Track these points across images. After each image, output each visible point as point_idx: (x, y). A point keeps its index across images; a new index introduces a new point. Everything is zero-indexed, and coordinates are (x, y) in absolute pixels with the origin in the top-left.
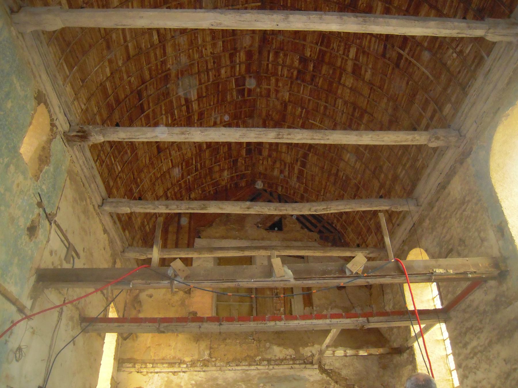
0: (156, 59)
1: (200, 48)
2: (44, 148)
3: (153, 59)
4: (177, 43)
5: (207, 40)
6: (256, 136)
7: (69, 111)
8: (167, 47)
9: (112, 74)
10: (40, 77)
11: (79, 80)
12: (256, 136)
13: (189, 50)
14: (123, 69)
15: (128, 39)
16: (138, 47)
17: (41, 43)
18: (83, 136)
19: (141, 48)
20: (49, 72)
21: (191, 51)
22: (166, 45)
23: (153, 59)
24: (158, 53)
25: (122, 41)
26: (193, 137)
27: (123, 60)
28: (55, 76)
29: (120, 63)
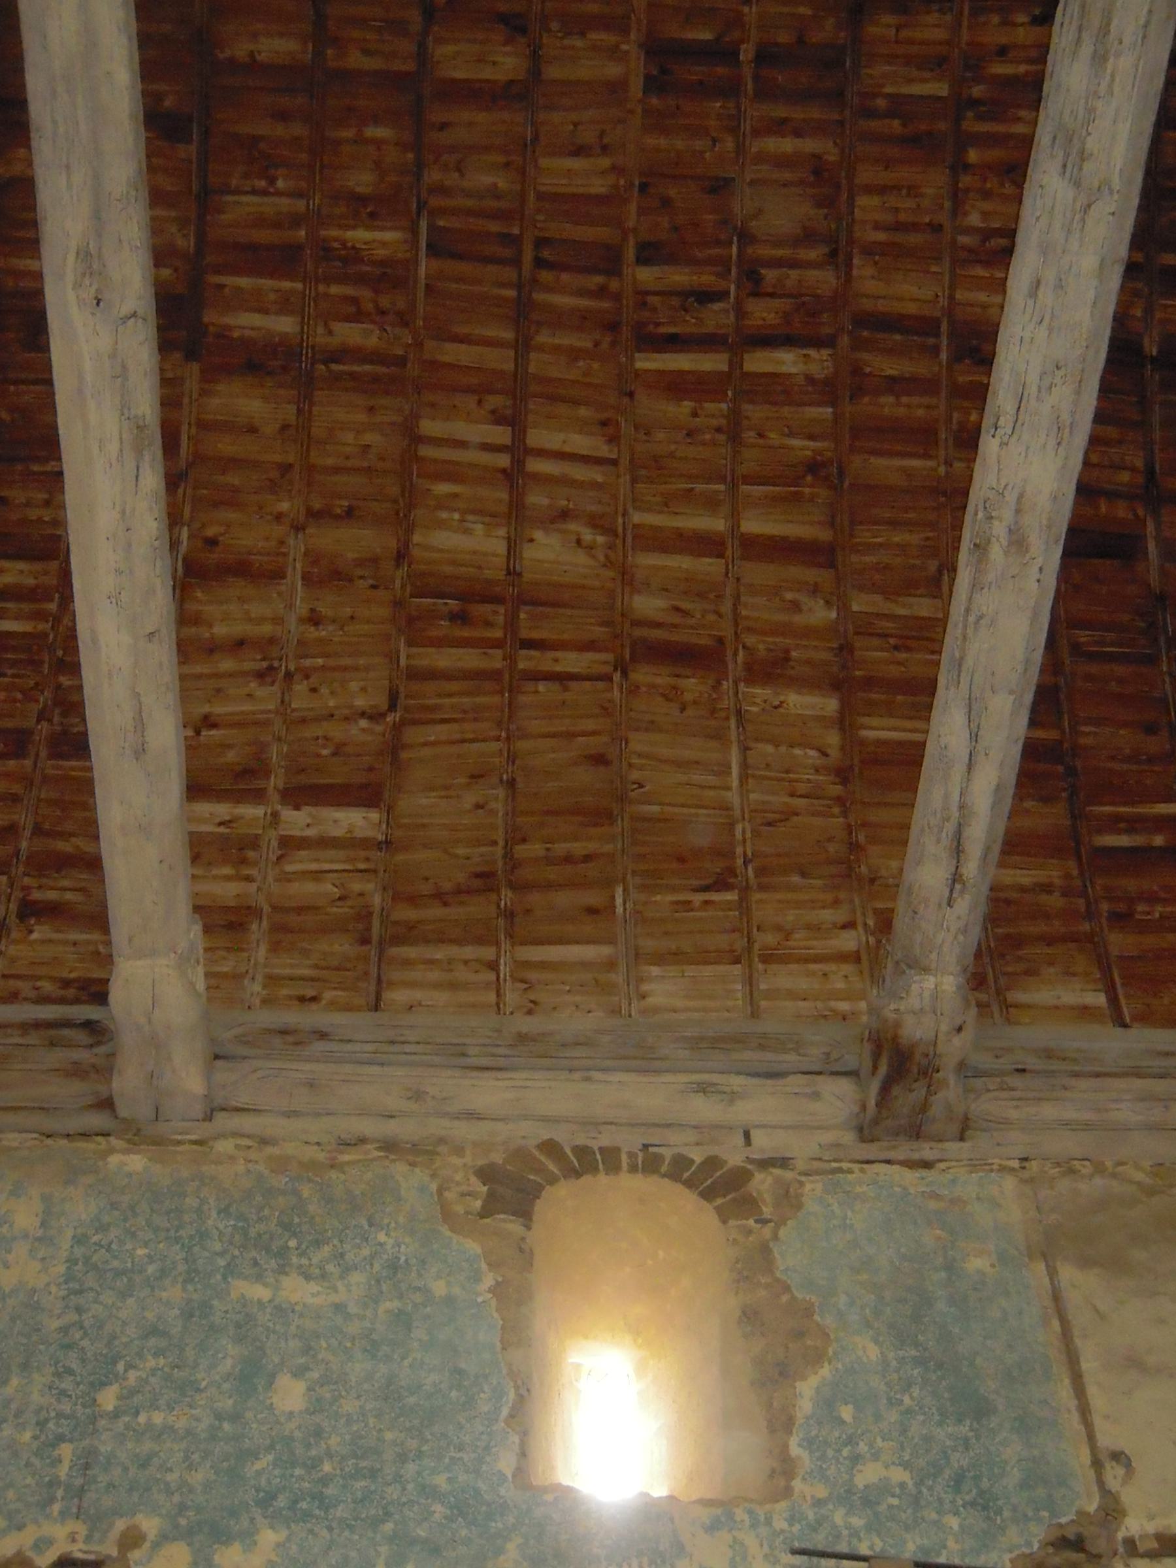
0: (927, 386)
1: (977, 91)
2: (750, 1316)
3: (914, 408)
4: (881, 236)
5: (940, 34)
6: (1087, 50)
7: (762, 1047)
8: (882, 306)
9: (837, 685)
10: (472, 1116)
11: (698, 898)
12: (1087, 50)
13: (967, 167)
14: (860, 603)
15: (717, 524)
16: (792, 480)
17: (323, 1035)
18: (897, 1065)
19: (814, 467)
20: (484, 1062)
21: (973, 156)
22: (867, 305)
23: (914, 408)
24: (891, 367)
25: (709, 566)
26: (1011, 497)
27: (815, 590)
28: (522, 1038)
29: (819, 614)
